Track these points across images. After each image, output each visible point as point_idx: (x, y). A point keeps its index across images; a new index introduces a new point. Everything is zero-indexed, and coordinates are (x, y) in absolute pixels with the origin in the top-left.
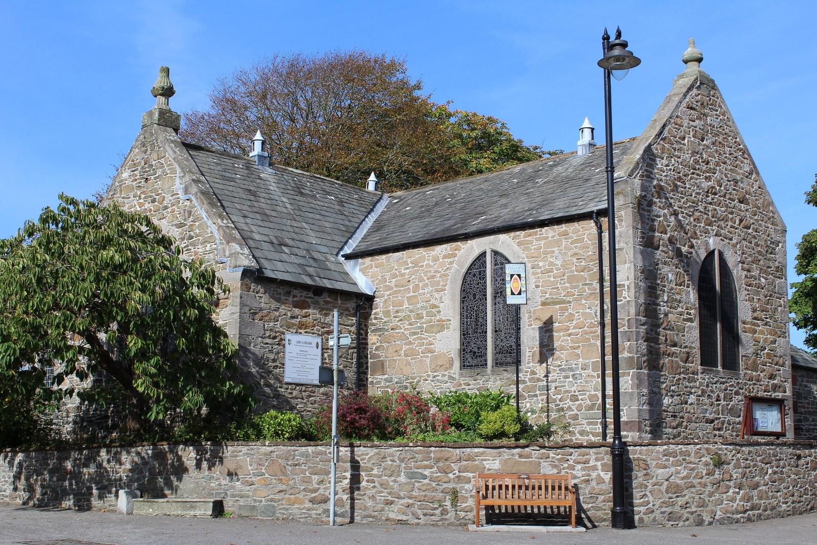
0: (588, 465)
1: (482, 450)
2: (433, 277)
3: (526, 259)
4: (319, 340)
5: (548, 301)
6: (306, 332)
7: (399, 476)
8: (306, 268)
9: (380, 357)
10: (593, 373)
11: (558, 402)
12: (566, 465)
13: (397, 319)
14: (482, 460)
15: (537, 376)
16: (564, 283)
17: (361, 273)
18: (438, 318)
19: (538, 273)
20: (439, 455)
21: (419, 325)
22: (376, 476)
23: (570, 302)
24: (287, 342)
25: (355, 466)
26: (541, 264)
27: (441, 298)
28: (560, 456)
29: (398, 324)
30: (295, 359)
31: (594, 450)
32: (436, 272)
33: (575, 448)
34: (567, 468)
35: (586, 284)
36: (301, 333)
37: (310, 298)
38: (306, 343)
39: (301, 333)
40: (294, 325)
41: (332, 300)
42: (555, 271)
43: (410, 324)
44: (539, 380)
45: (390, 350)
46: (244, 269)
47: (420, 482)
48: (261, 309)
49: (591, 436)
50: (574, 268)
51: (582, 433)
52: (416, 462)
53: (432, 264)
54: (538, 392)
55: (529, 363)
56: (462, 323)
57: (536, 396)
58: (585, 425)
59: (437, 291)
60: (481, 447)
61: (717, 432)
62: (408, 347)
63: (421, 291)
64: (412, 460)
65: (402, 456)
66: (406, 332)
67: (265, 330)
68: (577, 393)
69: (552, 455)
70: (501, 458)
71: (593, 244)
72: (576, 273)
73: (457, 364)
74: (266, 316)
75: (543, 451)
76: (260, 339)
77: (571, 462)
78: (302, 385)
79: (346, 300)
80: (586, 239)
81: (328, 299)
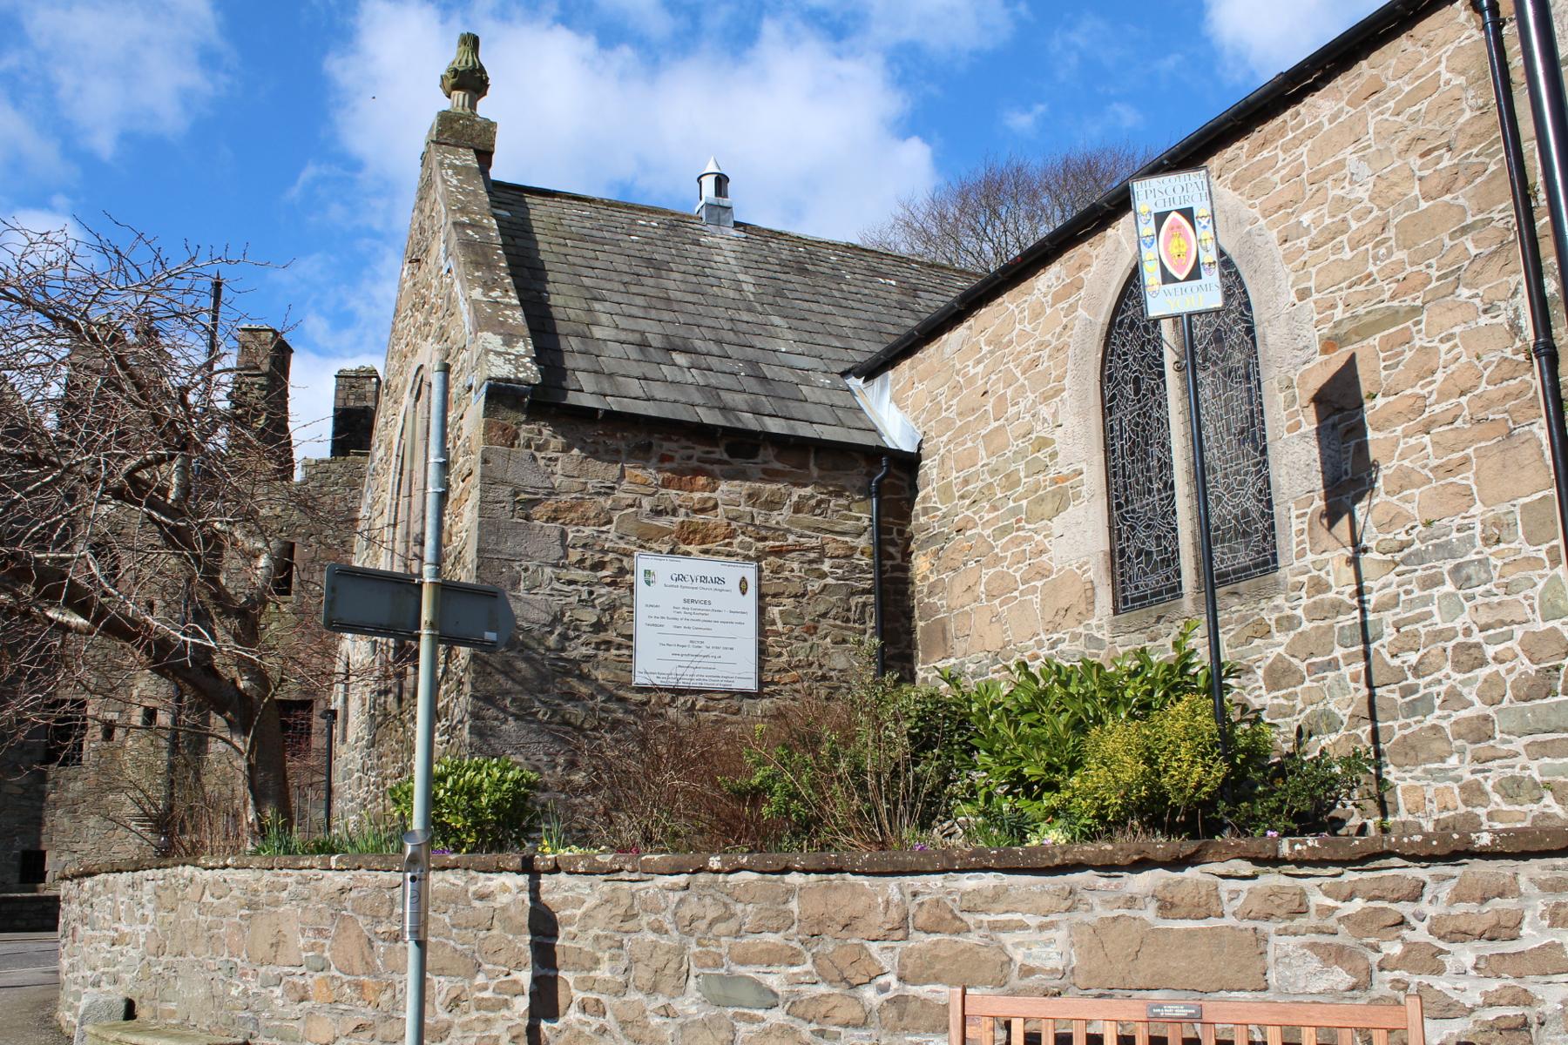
0: (1510, 947)
1: (990, 880)
2: (1035, 363)
3: (1262, 222)
4: (750, 572)
5: (1342, 331)
6: (706, 552)
7: (681, 990)
8: (722, 393)
9: (937, 611)
10: (1529, 550)
11: (1411, 680)
12: (1396, 949)
13: (967, 502)
14: (994, 927)
15: (1331, 595)
16: (1390, 253)
17: (893, 406)
18: (1052, 473)
19: (1301, 252)
20: (816, 907)
21: (1011, 504)
22: (606, 988)
23: (1416, 311)
24: (639, 580)
25: (543, 924)
26: (1306, 219)
27: (1055, 415)
28: (1358, 904)
29: (969, 513)
30: (669, 625)
31: (1535, 867)
32: (1042, 345)
33: (1432, 859)
34: (1401, 962)
35: (1464, 230)
36: (688, 554)
37: (719, 462)
38: (704, 579)
39: (688, 554)
40: (662, 532)
41: (788, 468)
42: (1354, 225)
43: (994, 508)
44: (1337, 608)
45: (958, 589)
46: (489, 387)
47: (752, 1020)
48: (552, 492)
49: (1549, 799)
50: (1416, 191)
51: (1513, 789)
52: (737, 934)
53: (1029, 328)
54: (1339, 652)
55: (1301, 554)
56: (1111, 473)
57: (1333, 665)
58: (1523, 759)
59: (1046, 399)
60: (986, 870)
61: (1286, 808)
62: (992, 571)
63: (1012, 410)
64: (721, 928)
65: (686, 912)
66: (985, 533)
67: (564, 546)
68: (1477, 637)
69: (1317, 899)
70: (1077, 916)
71: (1471, 83)
72: (1423, 205)
73: (1104, 598)
74: (571, 509)
75: (1272, 879)
76: (548, 570)
77: (1421, 934)
78: (699, 692)
79: (836, 468)
80: (1446, 75)
81: (778, 466)
